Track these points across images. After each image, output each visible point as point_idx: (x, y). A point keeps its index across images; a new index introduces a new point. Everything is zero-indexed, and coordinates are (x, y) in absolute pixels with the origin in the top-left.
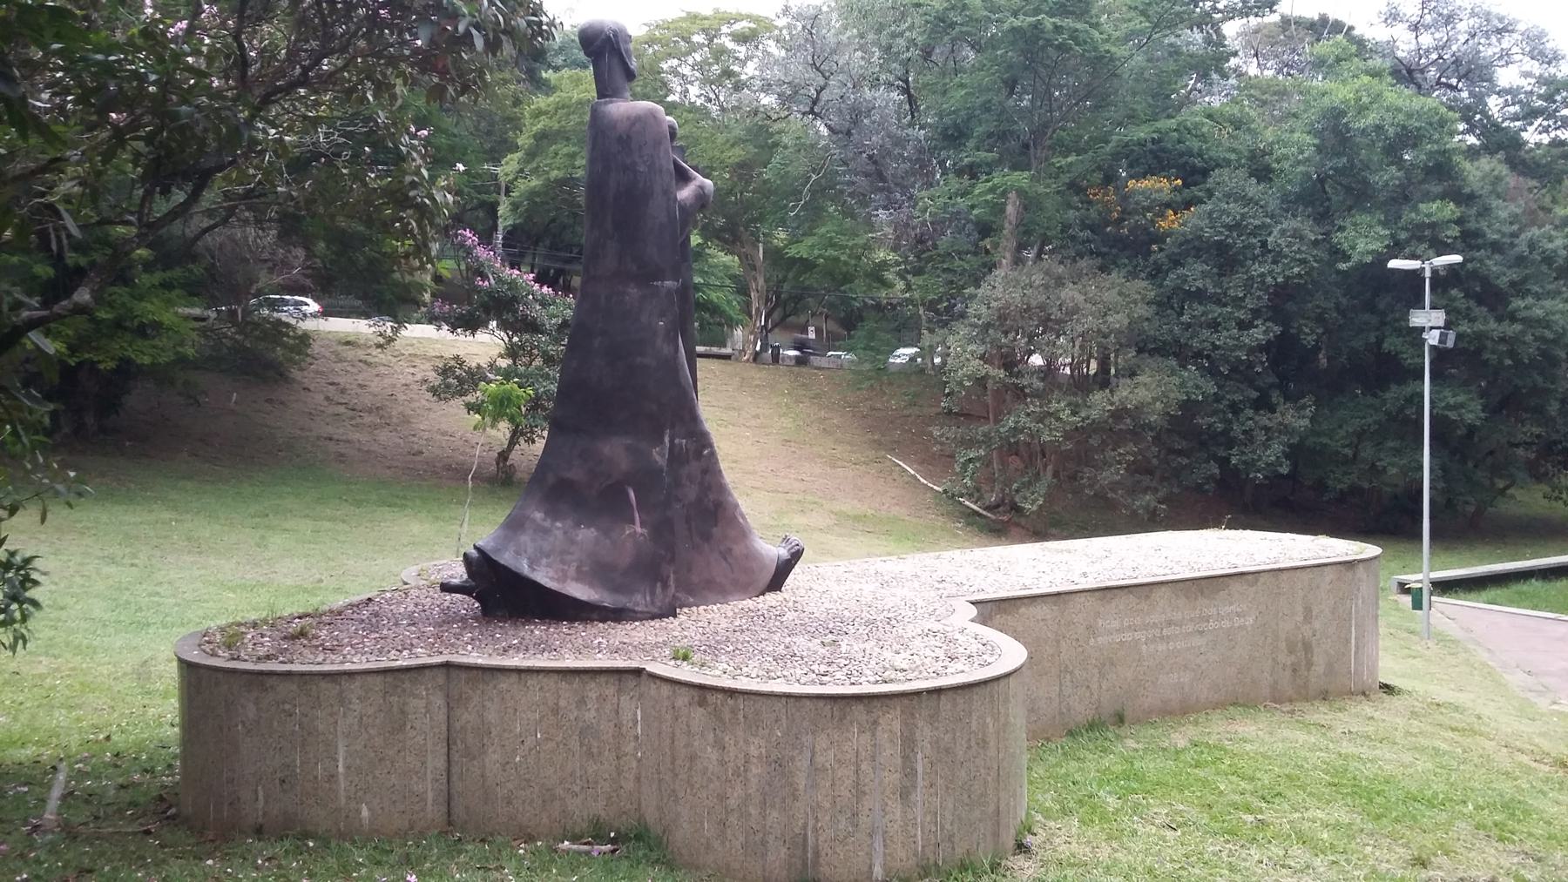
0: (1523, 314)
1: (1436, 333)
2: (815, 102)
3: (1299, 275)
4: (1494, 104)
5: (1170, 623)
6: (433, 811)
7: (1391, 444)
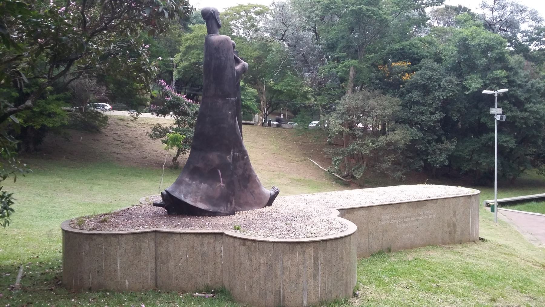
0: (529, 109)
1: (499, 116)
2: (283, 36)
3: (452, 96)
4: (519, 36)
5: (406, 217)
6: (151, 282)
7: (483, 155)
